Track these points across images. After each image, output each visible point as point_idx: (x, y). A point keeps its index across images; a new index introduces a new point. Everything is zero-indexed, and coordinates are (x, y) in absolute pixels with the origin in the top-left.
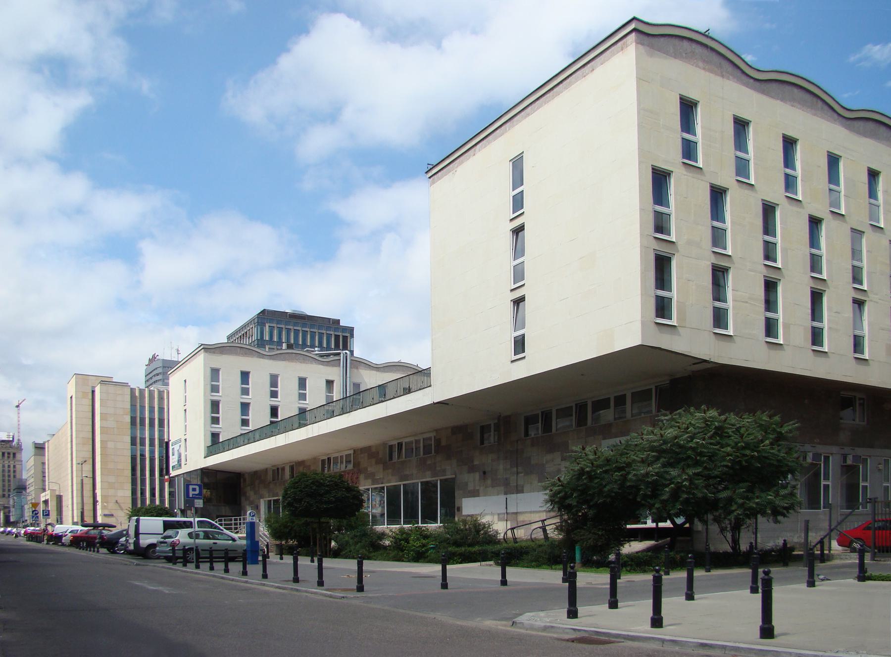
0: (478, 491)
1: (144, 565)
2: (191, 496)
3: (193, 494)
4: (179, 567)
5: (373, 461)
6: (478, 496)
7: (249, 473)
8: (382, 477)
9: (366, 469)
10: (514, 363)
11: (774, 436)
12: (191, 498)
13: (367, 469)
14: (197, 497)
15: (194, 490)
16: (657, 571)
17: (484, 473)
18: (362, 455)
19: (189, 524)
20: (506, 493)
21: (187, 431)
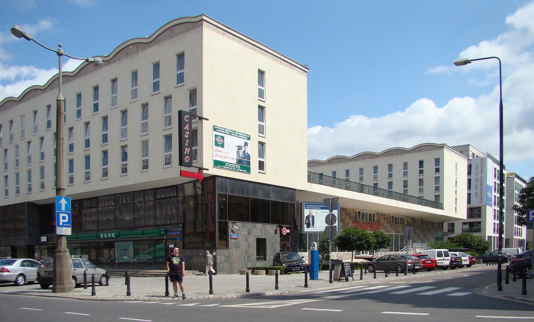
0: (416, 241)
1: (34, 289)
2: (531, 219)
3: (532, 218)
4: (82, 289)
5: (386, 221)
6: (416, 243)
7: (387, 214)
8: (389, 229)
9: (383, 224)
10: (66, 111)
11: (472, 234)
12: (531, 221)
13: (383, 224)
14: (67, 225)
15: (64, 218)
16: (499, 253)
17: (418, 235)
18: (382, 217)
19: (500, 230)
20: (422, 243)
21: (457, 170)
